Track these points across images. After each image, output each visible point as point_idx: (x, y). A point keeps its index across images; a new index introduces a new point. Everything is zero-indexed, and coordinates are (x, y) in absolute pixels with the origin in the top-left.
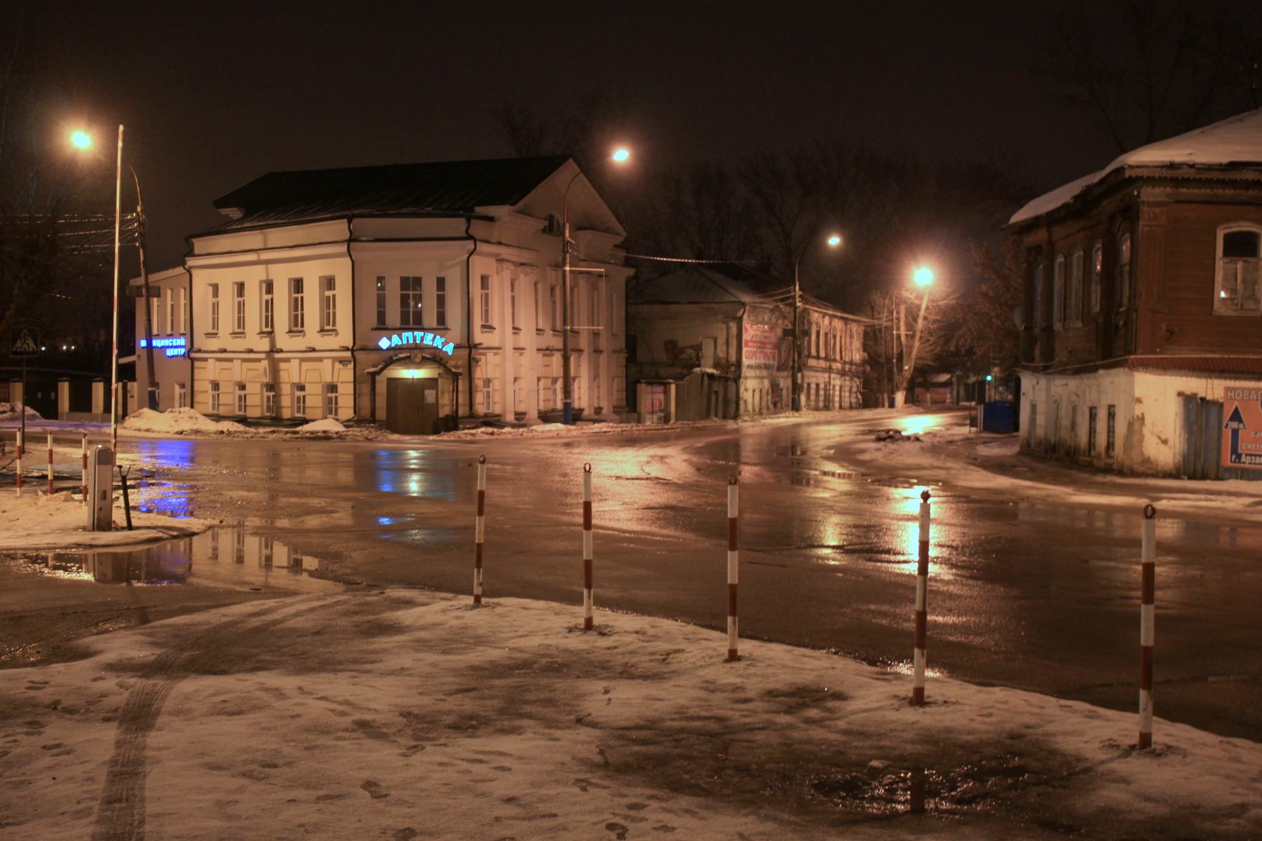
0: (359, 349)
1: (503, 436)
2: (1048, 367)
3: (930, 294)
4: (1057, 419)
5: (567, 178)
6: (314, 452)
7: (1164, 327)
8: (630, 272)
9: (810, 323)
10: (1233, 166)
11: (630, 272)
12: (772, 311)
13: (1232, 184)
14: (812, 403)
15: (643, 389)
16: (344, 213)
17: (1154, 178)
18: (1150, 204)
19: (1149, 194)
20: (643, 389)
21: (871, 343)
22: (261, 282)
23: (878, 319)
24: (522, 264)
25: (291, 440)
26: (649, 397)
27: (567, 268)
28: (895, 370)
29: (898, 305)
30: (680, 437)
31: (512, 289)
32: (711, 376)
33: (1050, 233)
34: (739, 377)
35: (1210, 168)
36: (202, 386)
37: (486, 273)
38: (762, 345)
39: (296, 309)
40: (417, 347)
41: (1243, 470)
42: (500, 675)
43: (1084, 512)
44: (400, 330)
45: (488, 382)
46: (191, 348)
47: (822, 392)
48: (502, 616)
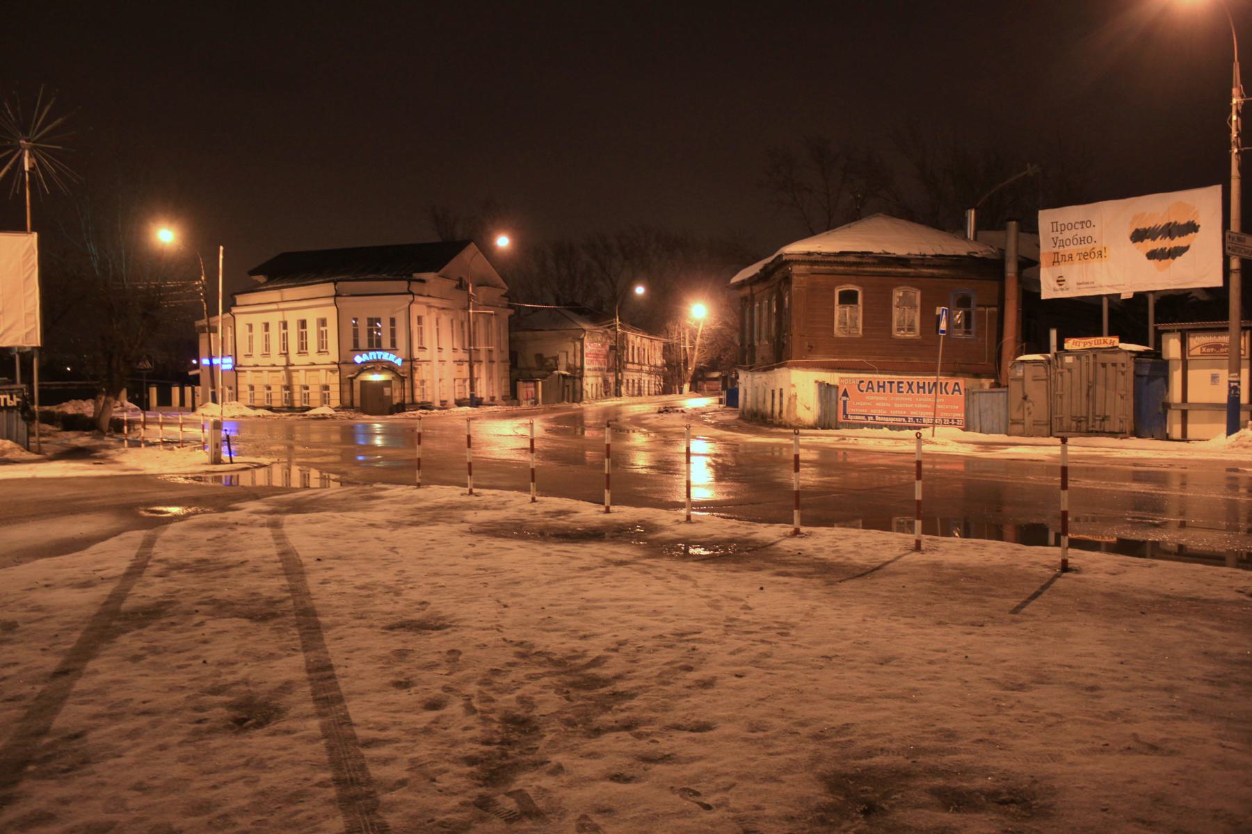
0: (343, 363)
1: (433, 415)
2: (752, 368)
3: (704, 322)
4: (757, 399)
5: (470, 254)
6: (315, 426)
7: (807, 344)
8: (511, 312)
9: (628, 342)
10: (842, 254)
11: (511, 312)
12: (603, 334)
13: (842, 263)
14: (630, 392)
15: (520, 384)
16: (331, 278)
17: (799, 261)
18: (797, 275)
19: (797, 269)
20: (520, 384)
21: (667, 353)
22: (280, 322)
23: (672, 338)
24: (443, 309)
25: (303, 420)
26: (525, 390)
27: (471, 311)
28: (683, 369)
29: (683, 329)
30: (544, 412)
31: (437, 324)
32: (564, 376)
33: (751, 290)
34: (582, 376)
35: (829, 255)
36: (243, 387)
37: (420, 314)
38: (597, 356)
39: (302, 339)
40: (378, 362)
41: (849, 423)
42: (429, 510)
43: (770, 448)
44: (368, 351)
45: (423, 382)
46: (235, 364)
47: (636, 385)
48: (430, 491)
